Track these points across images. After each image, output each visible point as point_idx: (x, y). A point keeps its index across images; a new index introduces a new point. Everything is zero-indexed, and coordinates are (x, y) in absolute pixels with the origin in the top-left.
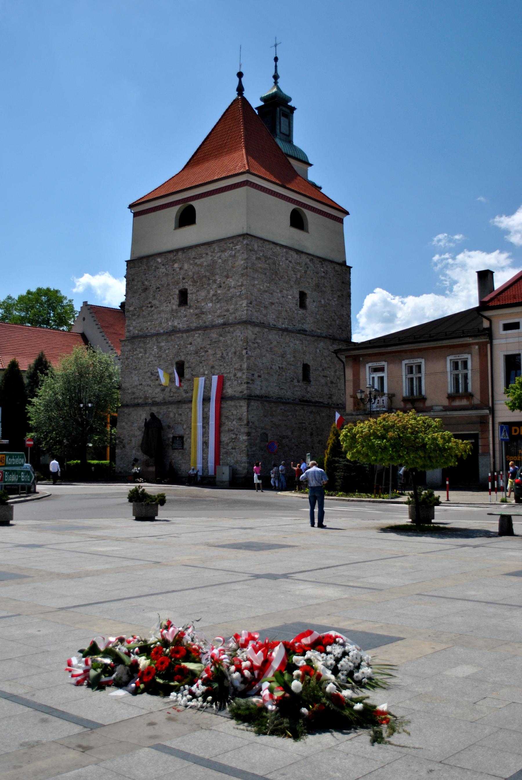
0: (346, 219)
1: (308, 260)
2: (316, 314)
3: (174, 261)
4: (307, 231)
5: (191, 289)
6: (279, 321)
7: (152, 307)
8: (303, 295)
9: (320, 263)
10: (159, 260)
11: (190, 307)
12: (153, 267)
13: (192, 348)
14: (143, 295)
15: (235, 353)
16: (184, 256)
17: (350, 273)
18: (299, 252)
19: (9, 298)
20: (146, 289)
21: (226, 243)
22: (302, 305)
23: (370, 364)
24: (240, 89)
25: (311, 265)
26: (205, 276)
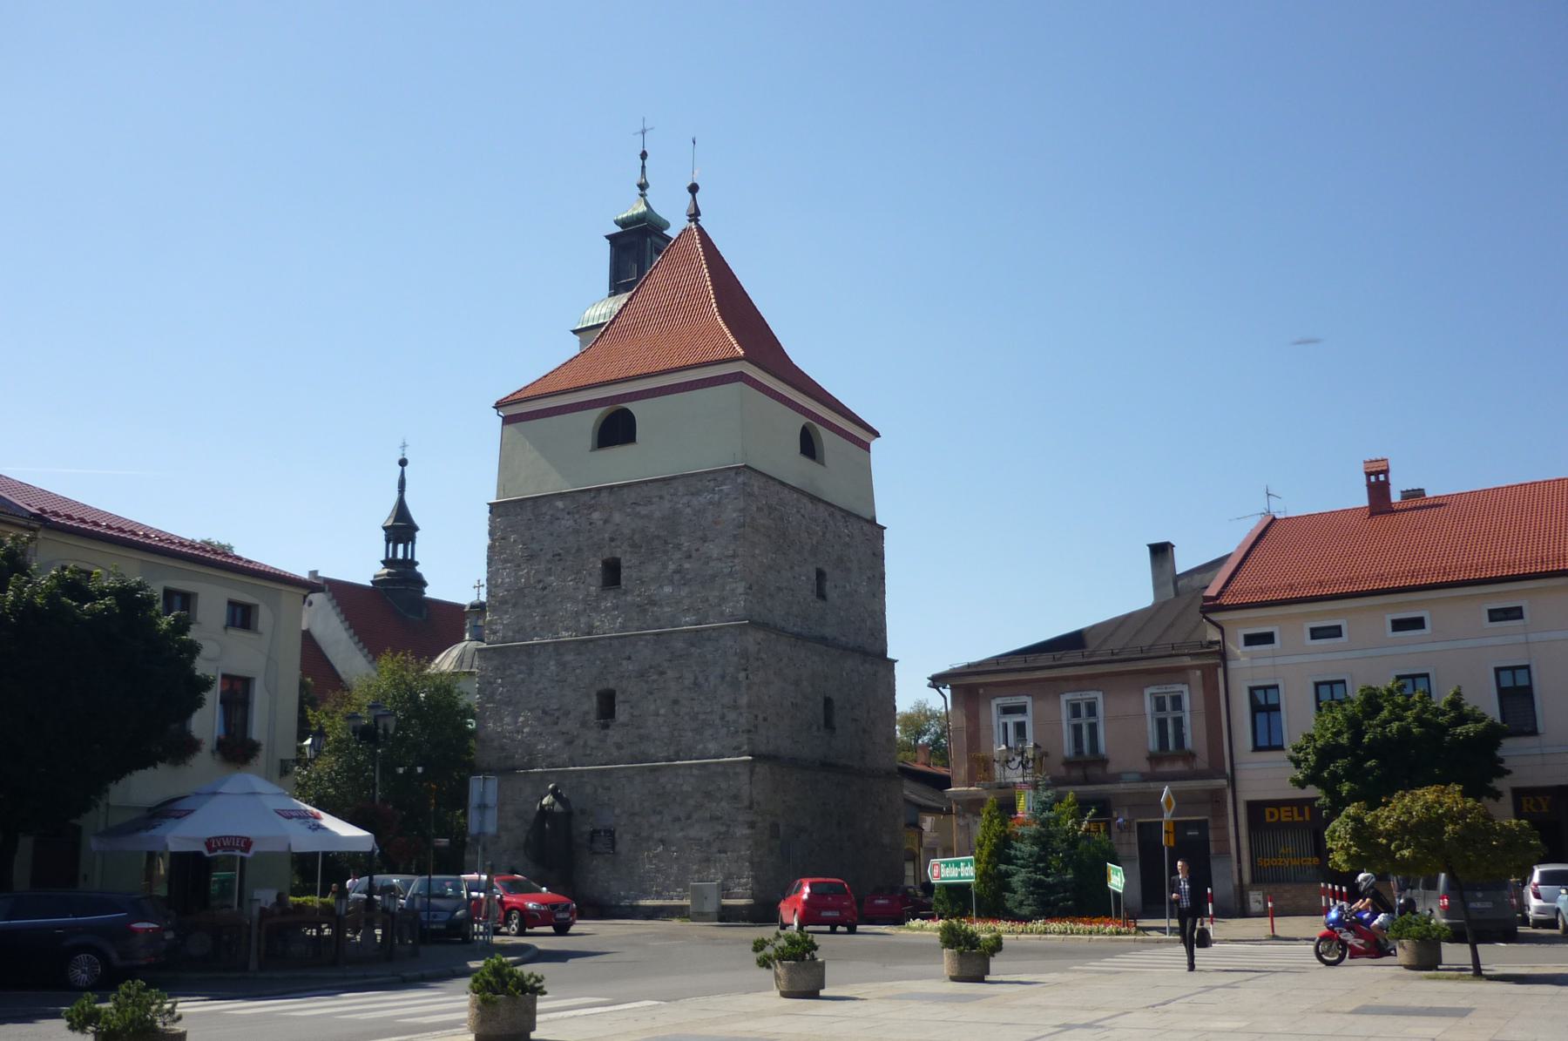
0: (875, 445)
3: (592, 508)
7: (544, 589)
8: (820, 574)
10: (560, 504)
13: (629, 667)
15: (723, 677)
18: (815, 499)
23: (999, 701)
26: (658, 537)
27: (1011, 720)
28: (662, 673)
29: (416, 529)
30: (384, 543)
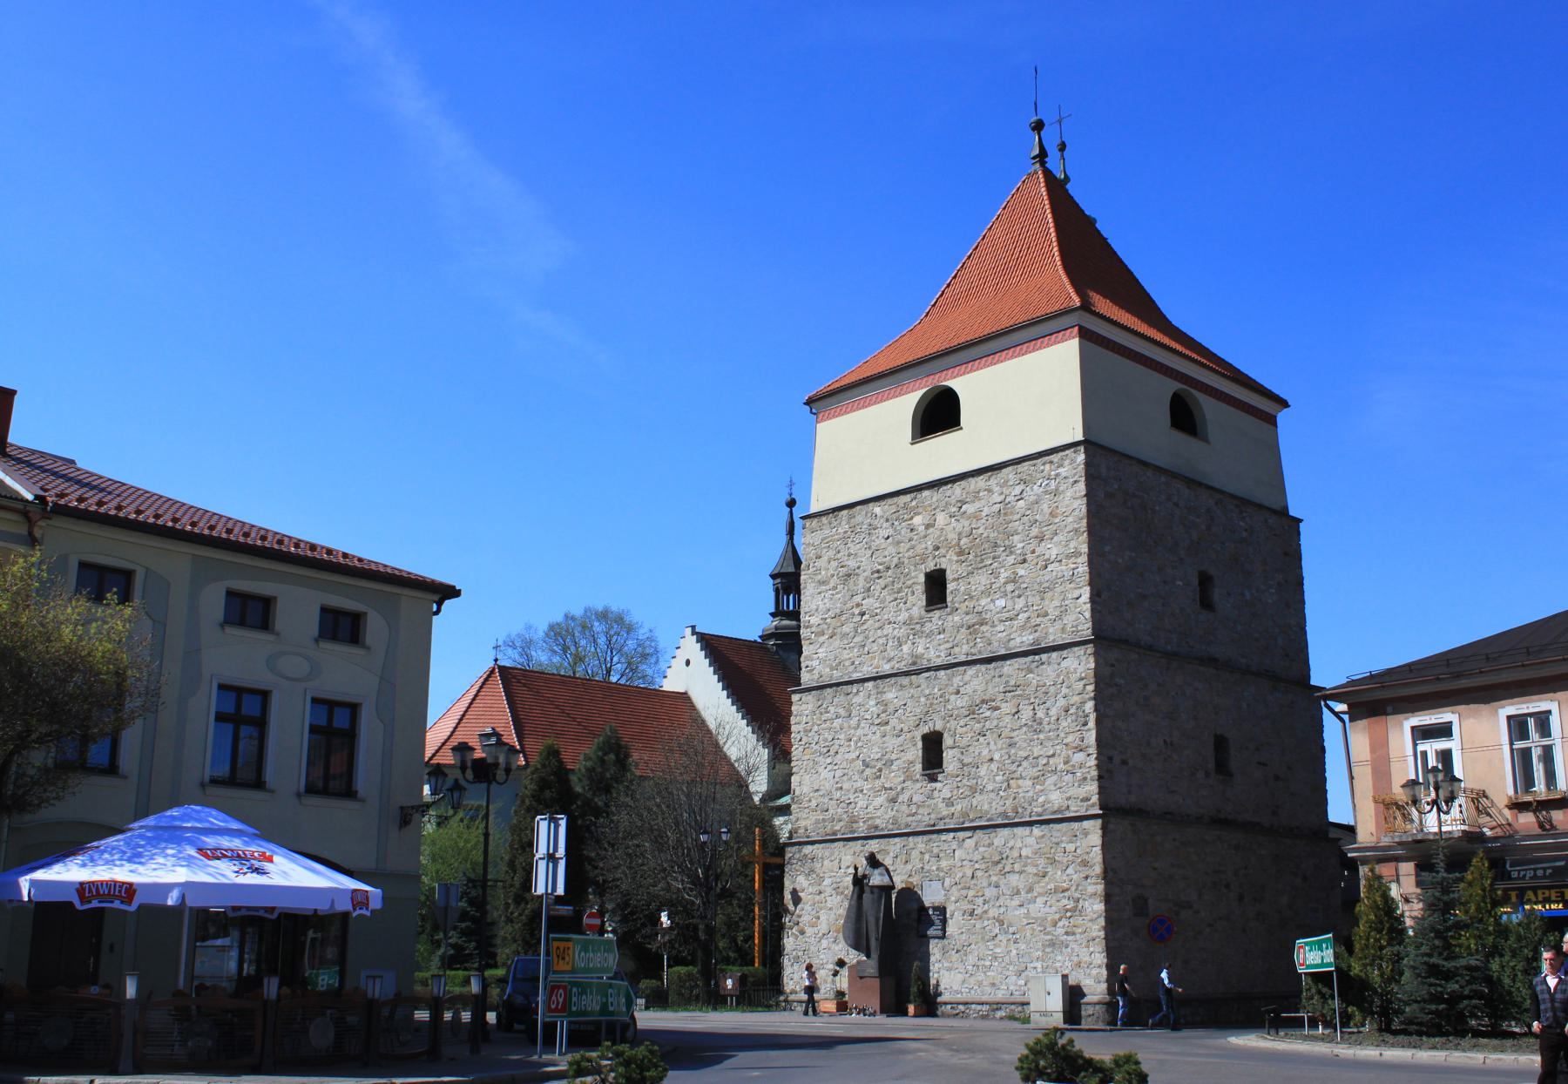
0: (1283, 417)
4: (1206, 440)
8: (1205, 581)
10: (877, 510)
18: (1193, 483)
19: (529, 627)
20: (849, 575)
22: (1206, 603)
27: (1431, 747)
30: (772, 595)
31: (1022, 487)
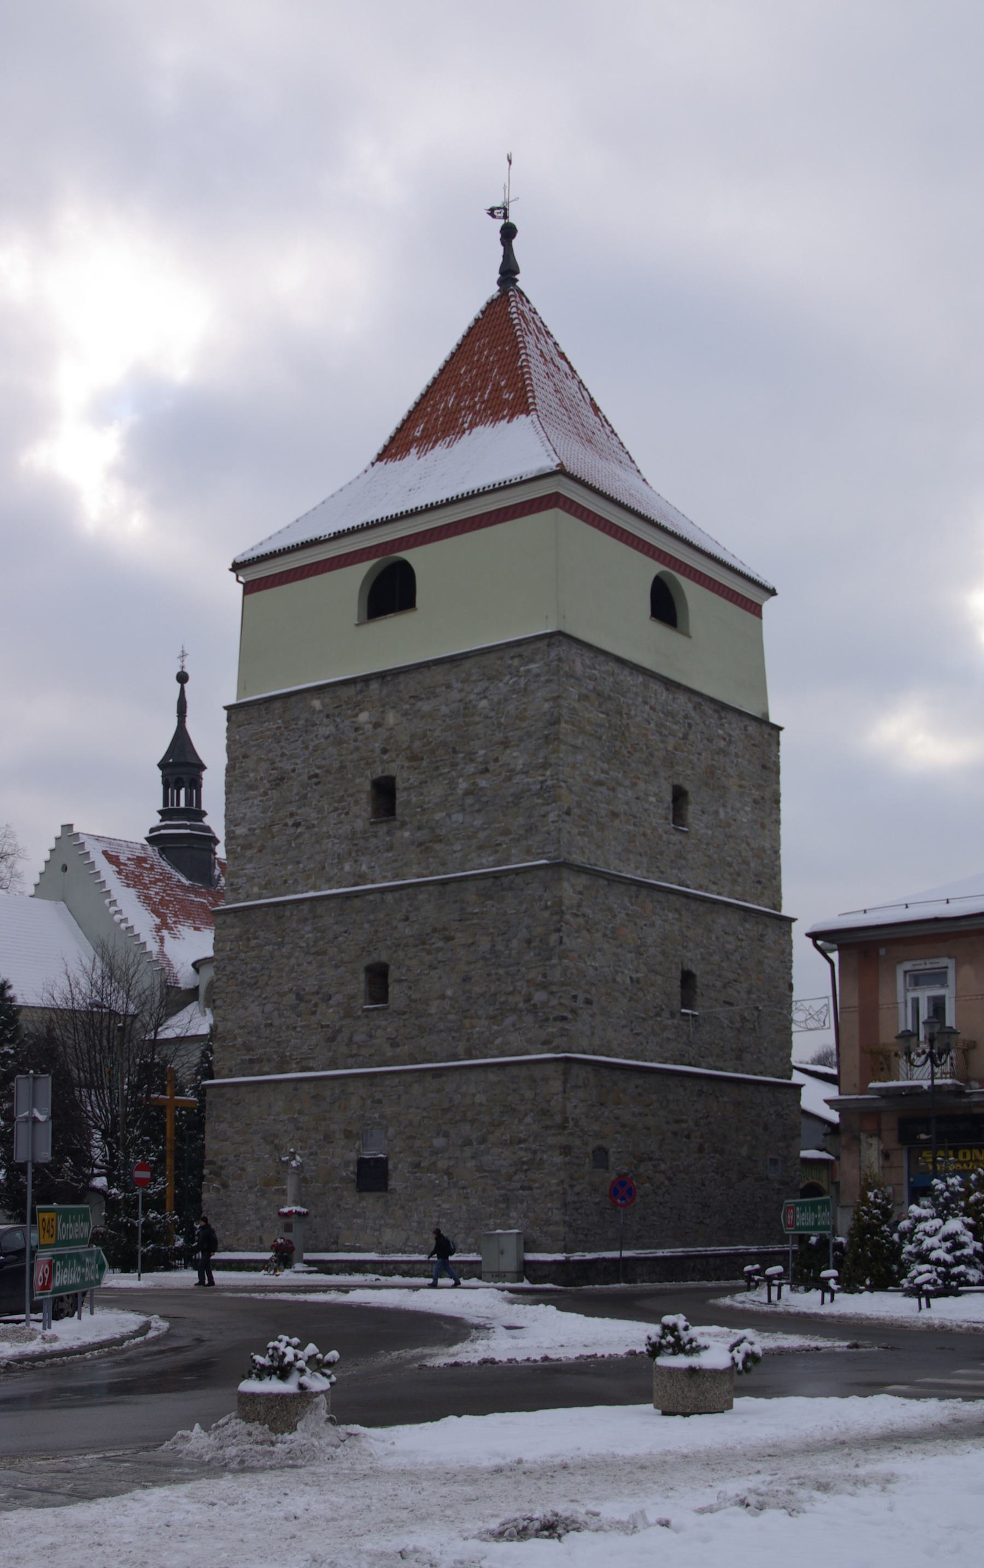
0: (769, 606)
1: (690, 706)
2: (708, 844)
3: (358, 707)
5: (404, 778)
6: (628, 860)
7: (297, 825)
8: (679, 795)
9: (716, 716)
10: (317, 704)
11: (403, 824)
12: (301, 722)
14: (274, 794)
16: (384, 692)
17: (778, 744)
18: (670, 684)
21: (501, 658)
23: (908, 966)
24: (509, 271)
25: (697, 718)
27: (924, 995)
28: (449, 939)
29: (203, 767)
31: (486, 684)
